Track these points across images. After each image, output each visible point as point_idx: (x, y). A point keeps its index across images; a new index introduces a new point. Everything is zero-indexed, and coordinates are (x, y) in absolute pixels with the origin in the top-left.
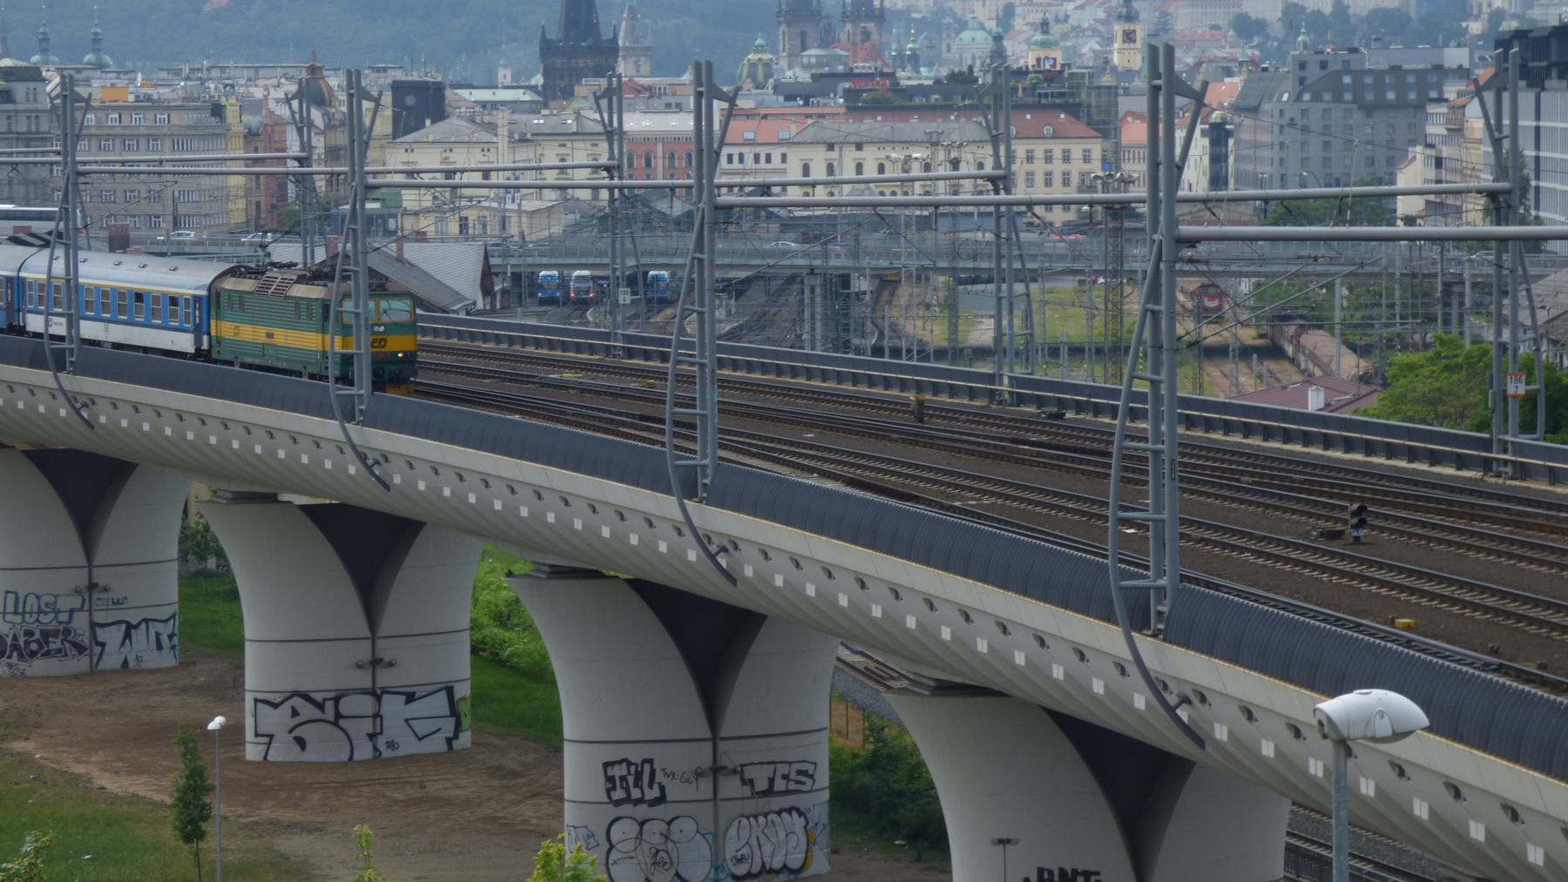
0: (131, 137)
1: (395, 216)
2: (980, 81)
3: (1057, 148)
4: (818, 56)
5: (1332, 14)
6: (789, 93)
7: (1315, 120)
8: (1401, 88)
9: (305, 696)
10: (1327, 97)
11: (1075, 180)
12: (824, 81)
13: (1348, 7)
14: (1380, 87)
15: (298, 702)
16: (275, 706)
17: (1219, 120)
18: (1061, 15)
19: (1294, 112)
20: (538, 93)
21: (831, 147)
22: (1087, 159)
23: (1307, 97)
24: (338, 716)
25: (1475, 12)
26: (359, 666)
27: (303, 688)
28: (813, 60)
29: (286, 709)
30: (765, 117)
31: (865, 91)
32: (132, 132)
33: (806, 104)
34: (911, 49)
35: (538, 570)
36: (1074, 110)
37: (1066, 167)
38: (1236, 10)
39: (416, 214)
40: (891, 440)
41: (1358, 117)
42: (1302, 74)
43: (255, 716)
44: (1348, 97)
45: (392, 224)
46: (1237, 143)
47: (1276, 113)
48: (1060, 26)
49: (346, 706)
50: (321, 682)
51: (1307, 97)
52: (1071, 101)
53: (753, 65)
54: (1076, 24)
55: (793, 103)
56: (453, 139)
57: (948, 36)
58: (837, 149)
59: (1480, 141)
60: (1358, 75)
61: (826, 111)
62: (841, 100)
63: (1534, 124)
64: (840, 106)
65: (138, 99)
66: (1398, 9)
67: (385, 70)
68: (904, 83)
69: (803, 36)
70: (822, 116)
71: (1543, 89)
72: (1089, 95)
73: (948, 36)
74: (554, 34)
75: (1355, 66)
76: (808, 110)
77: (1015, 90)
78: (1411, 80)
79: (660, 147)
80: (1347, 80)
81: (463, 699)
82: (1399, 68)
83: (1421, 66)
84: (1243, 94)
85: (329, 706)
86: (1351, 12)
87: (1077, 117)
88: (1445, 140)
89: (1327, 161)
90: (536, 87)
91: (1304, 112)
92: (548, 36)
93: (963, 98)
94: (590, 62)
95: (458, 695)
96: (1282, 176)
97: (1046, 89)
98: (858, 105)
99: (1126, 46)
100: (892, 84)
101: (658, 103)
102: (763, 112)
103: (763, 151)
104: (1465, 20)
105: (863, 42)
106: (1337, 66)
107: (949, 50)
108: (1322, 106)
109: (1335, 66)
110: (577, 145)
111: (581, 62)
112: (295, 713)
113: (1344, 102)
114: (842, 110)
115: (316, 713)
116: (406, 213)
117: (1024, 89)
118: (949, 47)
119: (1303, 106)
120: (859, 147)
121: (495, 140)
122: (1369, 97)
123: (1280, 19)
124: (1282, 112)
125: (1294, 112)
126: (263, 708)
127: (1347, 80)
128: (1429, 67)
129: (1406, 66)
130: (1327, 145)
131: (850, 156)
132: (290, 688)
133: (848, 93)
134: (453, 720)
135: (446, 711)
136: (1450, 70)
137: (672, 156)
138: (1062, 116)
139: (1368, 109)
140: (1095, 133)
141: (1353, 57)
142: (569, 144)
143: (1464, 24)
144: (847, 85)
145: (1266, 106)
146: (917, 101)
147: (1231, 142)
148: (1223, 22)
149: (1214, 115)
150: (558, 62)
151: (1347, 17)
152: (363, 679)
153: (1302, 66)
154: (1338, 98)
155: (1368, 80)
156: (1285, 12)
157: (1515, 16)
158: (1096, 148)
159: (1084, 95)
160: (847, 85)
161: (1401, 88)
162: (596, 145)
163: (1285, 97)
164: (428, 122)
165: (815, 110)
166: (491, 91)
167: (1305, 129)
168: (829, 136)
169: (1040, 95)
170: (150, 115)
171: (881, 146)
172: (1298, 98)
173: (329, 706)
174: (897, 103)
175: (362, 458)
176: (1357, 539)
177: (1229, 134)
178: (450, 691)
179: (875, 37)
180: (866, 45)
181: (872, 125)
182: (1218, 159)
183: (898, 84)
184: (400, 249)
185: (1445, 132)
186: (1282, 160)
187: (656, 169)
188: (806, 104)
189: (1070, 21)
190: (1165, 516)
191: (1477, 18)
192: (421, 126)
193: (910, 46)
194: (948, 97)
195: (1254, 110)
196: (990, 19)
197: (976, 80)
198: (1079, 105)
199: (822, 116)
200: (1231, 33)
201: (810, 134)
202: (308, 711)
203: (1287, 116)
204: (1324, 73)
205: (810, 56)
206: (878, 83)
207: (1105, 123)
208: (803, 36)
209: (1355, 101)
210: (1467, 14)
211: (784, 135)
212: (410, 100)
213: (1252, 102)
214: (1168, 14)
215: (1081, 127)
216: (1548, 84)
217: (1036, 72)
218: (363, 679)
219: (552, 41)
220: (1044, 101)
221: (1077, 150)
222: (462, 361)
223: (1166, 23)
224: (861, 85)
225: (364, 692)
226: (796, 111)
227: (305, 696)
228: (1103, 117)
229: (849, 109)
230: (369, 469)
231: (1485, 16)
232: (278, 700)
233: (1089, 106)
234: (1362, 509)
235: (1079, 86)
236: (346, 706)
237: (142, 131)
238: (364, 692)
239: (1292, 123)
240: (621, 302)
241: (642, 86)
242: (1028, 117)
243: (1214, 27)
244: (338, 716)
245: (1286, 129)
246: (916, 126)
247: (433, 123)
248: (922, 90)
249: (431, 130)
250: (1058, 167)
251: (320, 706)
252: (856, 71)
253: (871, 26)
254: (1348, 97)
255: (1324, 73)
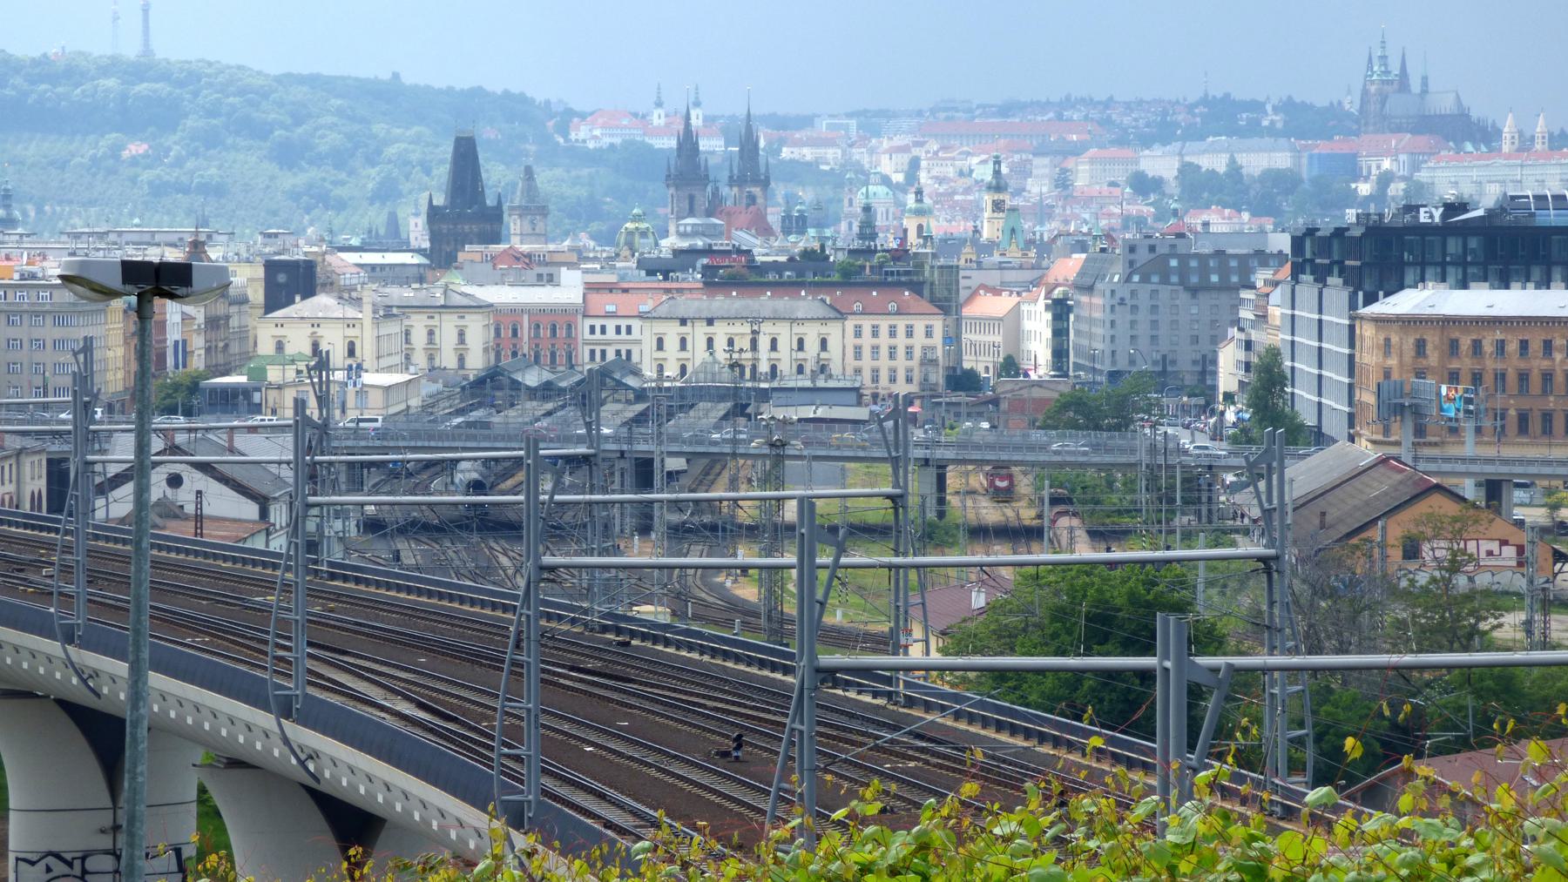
0: (15, 313)
1: (259, 390)
2: (832, 259)
3: (901, 323)
4: (693, 225)
5: (1227, 174)
6: (653, 268)
7: (1144, 300)
8: (1224, 272)
9: (57, 856)
10: (1155, 279)
11: (917, 353)
12: (684, 258)
13: (1241, 167)
14: (1204, 270)
15: (51, 860)
16: (33, 863)
17: (1061, 296)
18: (966, 170)
19: (1124, 292)
20: (425, 256)
21: (683, 322)
22: (929, 334)
23: (1136, 278)
24: (85, 872)
25: (1365, 173)
26: (103, 831)
27: (55, 849)
28: (689, 229)
29: (41, 866)
30: (626, 291)
31: (722, 267)
32: (15, 308)
33: (666, 278)
34: (798, 211)
35: (219, 761)
36: (917, 288)
37: (909, 341)
38: (1134, 168)
39: (279, 388)
40: (482, 665)
41: (1184, 297)
42: (1132, 257)
43: (16, 872)
44: (1174, 279)
45: (257, 397)
46: (1077, 318)
47: (1108, 293)
48: (963, 180)
49: (91, 864)
50: (71, 844)
51: (1136, 278)
52: (915, 278)
53: (630, 233)
54: (979, 178)
55: (653, 278)
56: (320, 315)
57: (850, 190)
58: (689, 324)
59: (1278, 328)
60: (1184, 259)
61: (685, 285)
62: (699, 276)
63: (1316, 317)
64: (698, 281)
65: (22, 278)
66: (1290, 170)
67: (276, 235)
68: (759, 259)
69: (692, 199)
70: (680, 290)
71: (1325, 285)
72: (932, 273)
73: (850, 190)
74: (439, 200)
75: (1181, 250)
76: (667, 285)
77: (863, 268)
78: (1234, 263)
79: (526, 318)
80: (1174, 263)
81: (190, 858)
82: (1223, 252)
83: (1244, 251)
84: (1082, 274)
85: (77, 864)
86: (1244, 171)
87: (920, 294)
88: (1254, 324)
89: (1154, 338)
90: (425, 250)
91: (1133, 293)
92: (435, 203)
93: (815, 275)
94: (475, 228)
95: (184, 856)
96: (1113, 352)
97: (891, 267)
98: (716, 281)
99: (996, 215)
100: (748, 261)
101: (531, 275)
102: (626, 285)
103: (623, 323)
104: (1355, 182)
105: (748, 206)
106: (1165, 250)
107: (851, 204)
108: (1149, 287)
109: (1162, 250)
110: (444, 317)
111: (467, 228)
112: (49, 870)
113: (1170, 284)
114: (700, 285)
115: (65, 869)
116: (270, 386)
117: (871, 267)
118: (851, 201)
119: (1133, 287)
120: (710, 322)
121: (360, 316)
122: (1194, 280)
123: (1176, 178)
124: (1113, 292)
125: (1124, 292)
126: (22, 865)
127: (1174, 263)
128: (1251, 252)
129: (1230, 251)
130: (1154, 324)
131: (699, 333)
132: (45, 849)
133: (706, 269)
134: (180, 875)
135: (174, 868)
136: (1272, 255)
137: (538, 326)
138: (907, 293)
139: (1194, 291)
140: (936, 310)
141: (1179, 242)
142: (437, 317)
143: (1353, 186)
144: (705, 261)
145: (1099, 286)
146: (771, 277)
147: (1072, 317)
148: (1121, 179)
149: (1056, 292)
150: (444, 227)
151: (1241, 176)
152: (106, 842)
153: (1132, 249)
154: (1165, 280)
155: (1194, 263)
156: (1180, 171)
157: (1403, 179)
158: (938, 324)
159: (927, 274)
160: (705, 261)
161: (1224, 272)
162: (463, 317)
163: (1116, 278)
164: (298, 298)
165: (675, 285)
166: (381, 254)
167: (1134, 308)
168: (682, 313)
169: (886, 273)
170: (33, 293)
171: (731, 322)
172: (1128, 279)
173: (77, 864)
174: (752, 280)
175: (79, 673)
176: (737, 757)
177: (1070, 309)
178: (178, 852)
179: (760, 201)
180: (752, 208)
181: (720, 303)
182: (1059, 333)
183: (754, 260)
184: (231, 440)
185: (1253, 317)
186: (1113, 337)
187: (522, 339)
188: (666, 278)
189: (974, 175)
190: (531, 753)
191: (1366, 179)
192: (291, 302)
193: (798, 207)
194: (800, 274)
195: (1089, 289)
196: (896, 172)
197: (827, 257)
198: (922, 283)
199: (680, 290)
200: (1128, 190)
201: (663, 311)
202: (58, 868)
203: (1118, 295)
204: (1152, 256)
205: (686, 225)
206: (735, 260)
207: (948, 300)
208: (692, 199)
209: (1181, 283)
210: (1357, 176)
211: (643, 308)
212: (282, 278)
213: (1088, 281)
214: (1068, 171)
215: (925, 305)
216: (1330, 280)
217: (884, 251)
218: (106, 842)
219: (438, 207)
220: (890, 279)
221: (919, 326)
222: (194, 582)
223: (1065, 179)
224: (718, 261)
225: (106, 852)
226: (655, 285)
227: (57, 856)
228: (946, 293)
229: (705, 283)
230: (85, 681)
231: (1373, 178)
232: (35, 859)
233: (932, 284)
234: (740, 736)
235: (922, 265)
236: (91, 864)
237: (25, 307)
238: (106, 852)
239: (1122, 302)
240: (326, 534)
241: (522, 253)
242: (875, 293)
243: (1113, 184)
244: (85, 872)
245: (1117, 307)
246: (766, 302)
247: (303, 298)
248: (776, 267)
249: (301, 307)
250: (901, 341)
251: (70, 864)
252: (715, 248)
253: (756, 190)
254: (1174, 279)
255: (1152, 256)
